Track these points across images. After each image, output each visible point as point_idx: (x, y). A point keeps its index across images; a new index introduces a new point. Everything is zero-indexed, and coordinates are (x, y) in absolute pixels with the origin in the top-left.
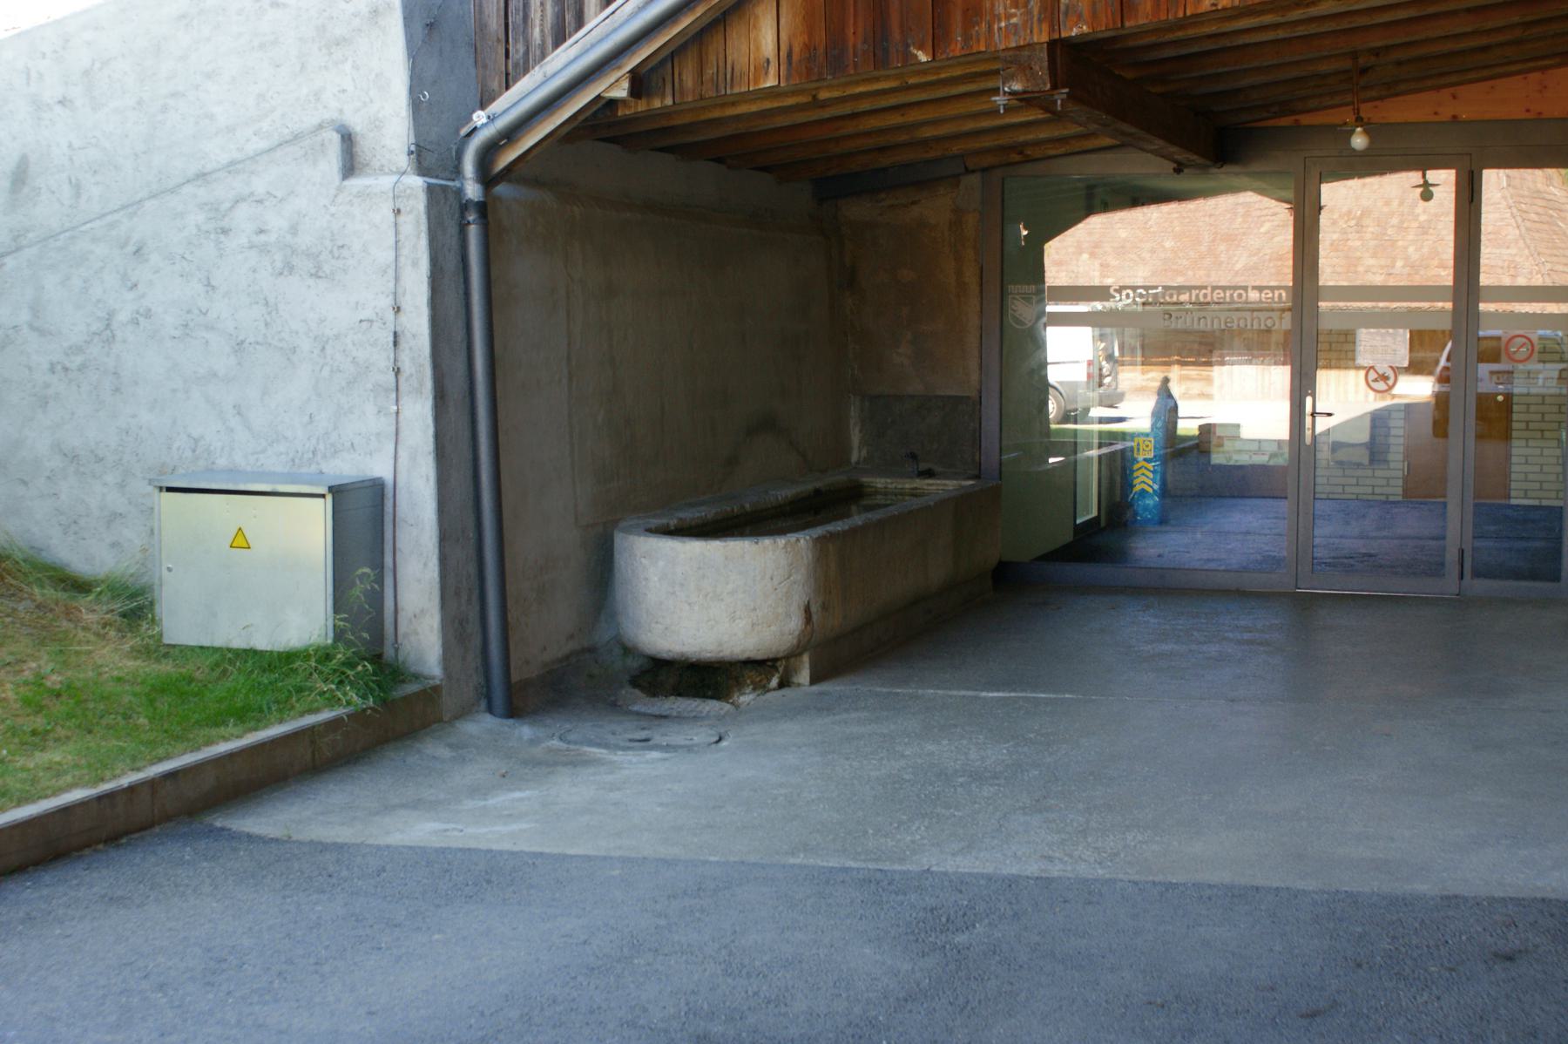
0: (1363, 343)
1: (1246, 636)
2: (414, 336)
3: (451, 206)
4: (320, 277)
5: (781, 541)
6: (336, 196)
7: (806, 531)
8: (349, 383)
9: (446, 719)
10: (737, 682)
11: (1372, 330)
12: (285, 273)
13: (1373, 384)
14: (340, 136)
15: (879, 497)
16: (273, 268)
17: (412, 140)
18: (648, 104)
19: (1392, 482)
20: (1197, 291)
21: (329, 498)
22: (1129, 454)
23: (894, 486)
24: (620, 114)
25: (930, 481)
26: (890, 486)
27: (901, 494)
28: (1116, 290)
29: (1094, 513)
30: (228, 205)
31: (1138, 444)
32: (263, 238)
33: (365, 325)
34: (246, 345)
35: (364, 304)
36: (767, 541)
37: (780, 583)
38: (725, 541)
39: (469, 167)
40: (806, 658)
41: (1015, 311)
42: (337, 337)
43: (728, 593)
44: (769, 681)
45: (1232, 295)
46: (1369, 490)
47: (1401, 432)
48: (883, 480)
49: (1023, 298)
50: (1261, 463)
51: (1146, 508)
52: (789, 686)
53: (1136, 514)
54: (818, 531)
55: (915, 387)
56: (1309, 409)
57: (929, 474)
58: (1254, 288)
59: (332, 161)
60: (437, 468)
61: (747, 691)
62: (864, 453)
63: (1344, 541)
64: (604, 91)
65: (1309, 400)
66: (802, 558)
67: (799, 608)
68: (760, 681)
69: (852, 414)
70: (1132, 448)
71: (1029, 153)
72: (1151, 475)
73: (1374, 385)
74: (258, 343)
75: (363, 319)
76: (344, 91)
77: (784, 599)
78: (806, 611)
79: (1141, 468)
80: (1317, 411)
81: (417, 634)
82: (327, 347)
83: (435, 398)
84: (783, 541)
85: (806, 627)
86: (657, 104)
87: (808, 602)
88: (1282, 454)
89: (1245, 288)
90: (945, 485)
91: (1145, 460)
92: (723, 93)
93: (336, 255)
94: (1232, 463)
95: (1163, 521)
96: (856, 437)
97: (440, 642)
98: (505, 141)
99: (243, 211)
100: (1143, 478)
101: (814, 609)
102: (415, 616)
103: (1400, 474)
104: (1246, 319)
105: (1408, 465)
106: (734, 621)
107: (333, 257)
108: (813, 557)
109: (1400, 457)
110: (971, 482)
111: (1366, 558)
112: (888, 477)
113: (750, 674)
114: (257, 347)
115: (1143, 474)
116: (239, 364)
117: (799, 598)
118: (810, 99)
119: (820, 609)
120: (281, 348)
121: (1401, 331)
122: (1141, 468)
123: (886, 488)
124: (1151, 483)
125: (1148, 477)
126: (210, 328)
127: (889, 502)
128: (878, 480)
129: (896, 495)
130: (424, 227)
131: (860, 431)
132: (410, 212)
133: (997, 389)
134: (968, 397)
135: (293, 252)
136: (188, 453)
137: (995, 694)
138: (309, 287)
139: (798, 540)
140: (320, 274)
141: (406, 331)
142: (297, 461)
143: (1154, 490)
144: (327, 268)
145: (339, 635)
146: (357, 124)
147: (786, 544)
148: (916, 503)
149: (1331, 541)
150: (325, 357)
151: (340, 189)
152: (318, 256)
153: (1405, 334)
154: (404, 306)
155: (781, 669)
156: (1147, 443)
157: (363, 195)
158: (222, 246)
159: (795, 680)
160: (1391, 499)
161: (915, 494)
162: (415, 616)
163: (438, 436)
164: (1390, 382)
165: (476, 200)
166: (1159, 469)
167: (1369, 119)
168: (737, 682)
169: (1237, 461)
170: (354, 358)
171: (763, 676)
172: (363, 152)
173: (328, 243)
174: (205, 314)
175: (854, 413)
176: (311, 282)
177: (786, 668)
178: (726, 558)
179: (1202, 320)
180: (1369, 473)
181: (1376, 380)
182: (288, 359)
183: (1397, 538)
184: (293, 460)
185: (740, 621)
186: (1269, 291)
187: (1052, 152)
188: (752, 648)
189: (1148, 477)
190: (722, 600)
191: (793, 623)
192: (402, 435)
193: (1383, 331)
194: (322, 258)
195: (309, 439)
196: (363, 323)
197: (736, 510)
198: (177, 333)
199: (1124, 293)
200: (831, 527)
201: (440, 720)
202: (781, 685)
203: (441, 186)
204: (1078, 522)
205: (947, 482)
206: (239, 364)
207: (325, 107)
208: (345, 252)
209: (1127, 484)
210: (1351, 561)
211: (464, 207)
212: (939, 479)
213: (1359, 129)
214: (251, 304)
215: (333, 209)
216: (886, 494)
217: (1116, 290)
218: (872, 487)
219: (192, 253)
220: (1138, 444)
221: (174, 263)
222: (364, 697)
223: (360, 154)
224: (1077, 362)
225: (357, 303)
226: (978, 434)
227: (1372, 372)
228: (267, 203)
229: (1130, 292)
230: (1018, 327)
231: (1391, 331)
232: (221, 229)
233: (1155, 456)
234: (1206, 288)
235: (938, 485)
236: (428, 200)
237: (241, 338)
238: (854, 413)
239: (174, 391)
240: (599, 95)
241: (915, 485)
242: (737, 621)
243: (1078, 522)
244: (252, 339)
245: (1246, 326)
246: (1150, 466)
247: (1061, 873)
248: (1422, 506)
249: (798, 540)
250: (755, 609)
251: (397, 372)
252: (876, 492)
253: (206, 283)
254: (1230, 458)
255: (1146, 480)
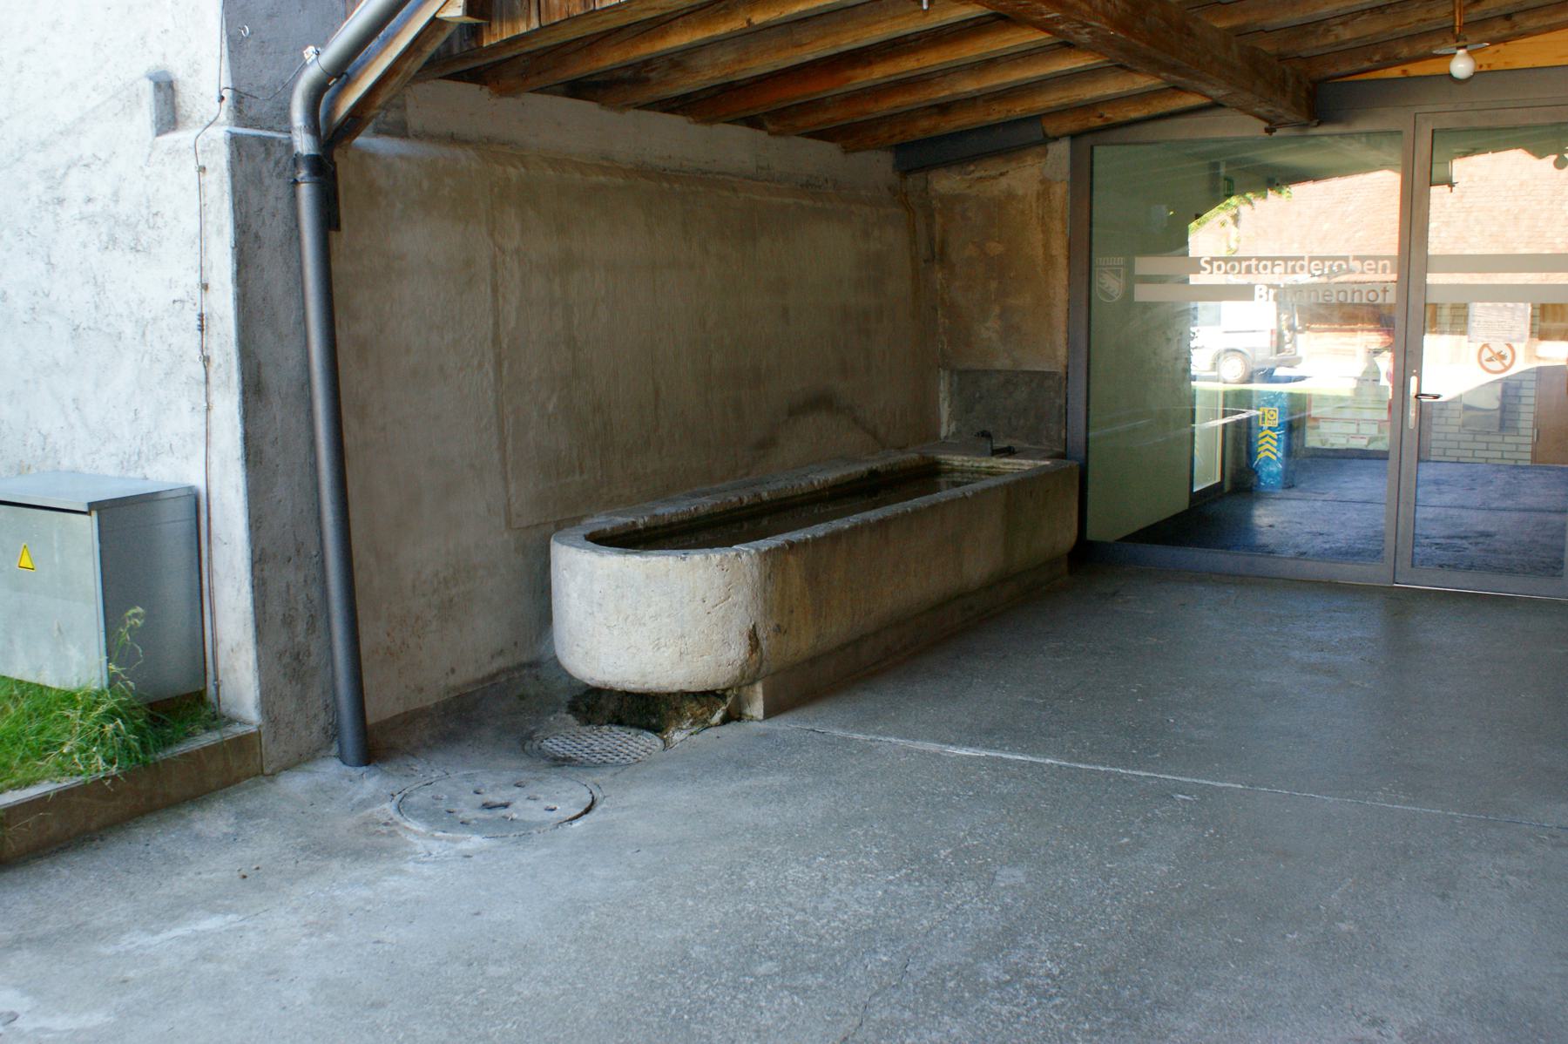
0: (1477, 319)
1: (1315, 657)
2: (221, 319)
3: (277, 163)
4: (138, 251)
5: (716, 556)
6: (150, 155)
7: (751, 544)
8: (166, 374)
9: (267, 771)
10: (678, 713)
11: (1488, 304)
12: (110, 247)
13: (1486, 364)
14: (152, 83)
15: (956, 474)
16: (100, 242)
17: (226, 81)
18: (513, 29)
19: (1522, 448)
20: (1293, 263)
21: (94, 514)
22: (1253, 423)
23: (970, 463)
24: (485, 45)
25: (1006, 460)
26: (966, 464)
27: (977, 472)
28: (1206, 262)
29: (1218, 479)
30: (62, 171)
31: (1264, 414)
32: (91, 208)
33: (178, 305)
34: (80, 330)
35: (176, 282)
36: (697, 557)
37: (713, 607)
38: (646, 557)
39: (298, 115)
40: (759, 688)
41: (1102, 284)
42: (155, 320)
43: (651, 617)
44: (712, 714)
45: (1331, 267)
46: (1499, 455)
47: (1533, 393)
48: (960, 458)
49: (1111, 271)
50: (1360, 447)
51: (1269, 475)
52: (739, 719)
53: (1259, 480)
54: (766, 544)
55: (1002, 363)
56: (1413, 390)
57: (1009, 452)
58: (1356, 258)
59: (145, 115)
60: (247, 476)
61: (684, 727)
62: (953, 428)
63: (1464, 513)
64: (438, 11)
65: (1413, 381)
66: (745, 576)
67: (741, 634)
68: (702, 714)
69: (942, 388)
70: (1257, 417)
71: (1109, 115)
72: (1275, 443)
73: (1491, 366)
74: (90, 328)
75: (176, 299)
76: (166, 31)
77: (720, 624)
78: (750, 638)
79: (1265, 436)
80: (1423, 392)
81: (235, 670)
82: (147, 332)
83: (244, 393)
84: (718, 557)
85: (751, 655)
86: (522, 29)
87: (754, 626)
88: (1382, 438)
89: (1346, 259)
90: (1022, 465)
91: (1270, 428)
92: (592, 8)
93: (151, 225)
94: (1328, 446)
95: (1289, 485)
96: (945, 411)
97: (257, 682)
98: (335, 80)
99: (75, 177)
100: (1267, 446)
101: (761, 634)
102: (232, 650)
103: (1529, 440)
104: (1346, 292)
105: (1538, 432)
106: (659, 649)
107: (149, 227)
108: (760, 574)
109: (1530, 424)
110: (1047, 463)
111: (1481, 540)
112: (966, 455)
113: (691, 708)
114: (90, 332)
115: (1268, 442)
116: (76, 352)
117: (740, 622)
118: (745, 25)
119: (771, 634)
120: (109, 334)
121: (1522, 305)
122: (1265, 436)
123: (962, 465)
124: (1275, 451)
125: (1272, 445)
126: (52, 312)
127: (965, 480)
128: (955, 458)
129: (972, 473)
130: (227, 187)
131: (949, 406)
132: (214, 170)
133: (1084, 365)
134: (1055, 374)
135: (116, 222)
136: (39, 452)
137: (964, 752)
138: (130, 262)
139: (738, 555)
140: (140, 248)
141: (214, 315)
142: (125, 464)
143: (1278, 458)
144: (144, 240)
145: (113, 679)
146: (179, 71)
147: (721, 560)
148: (992, 482)
149: (1452, 512)
150: (146, 345)
151: (153, 147)
152: (136, 227)
153: (1526, 309)
154: (211, 284)
155: (729, 700)
156: (1272, 412)
157: (173, 152)
158: (58, 219)
159: (748, 711)
160: (1520, 463)
161: (991, 473)
162: (232, 650)
163: (247, 438)
164: (1507, 362)
165: (305, 153)
166: (1282, 437)
167: (1489, 65)
168: (678, 713)
169: (1333, 444)
170: (170, 345)
171: (705, 708)
172: (184, 102)
173: (144, 211)
174: (48, 296)
175: (943, 387)
176: (131, 256)
177: (737, 699)
178: (648, 577)
179: (1356, 294)
180: (1499, 439)
181: (1490, 360)
182: (116, 347)
183: (1520, 510)
184: (122, 462)
185: (665, 649)
186: (1371, 262)
187: (1134, 115)
188: (681, 681)
189: (1272, 445)
190: (644, 624)
191: (732, 651)
192: (214, 438)
193: (1500, 305)
194: (140, 228)
195: (134, 438)
196: (177, 304)
197: (746, 500)
198: (26, 318)
199: (1215, 264)
200: (797, 536)
201: (260, 773)
202: (726, 720)
203: (259, 137)
204: (1195, 490)
205: (1023, 461)
206: (76, 352)
207: (150, 52)
208: (160, 221)
209: (1251, 453)
210: (1465, 543)
211: (296, 160)
212: (1017, 458)
213: (1461, 52)
214: (83, 284)
215: (148, 171)
216: (962, 472)
217: (1206, 262)
218: (948, 464)
219: (35, 227)
220: (1264, 414)
221: (22, 240)
222: (111, 762)
223: (182, 104)
224: (1254, 331)
225: (170, 280)
226: (1064, 411)
227: (1486, 350)
228: (93, 167)
229: (1237, 264)
230: (1104, 300)
231: (1510, 305)
232: (58, 199)
233: (1279, 425)
234: (1302, 258)
235: (1014, 464)
236: (232, 154)
237: (77, 322)
238: (943, 387)
239: (26, 381)
240: (434, 19)
241: (991, 464)
242: (662, 649)
243: (1195, 490)
244: (84, 325)
245: (1346, 299)
246: (1274, 435)
247: (1442, 510)
248: (1550, 472)
249: (738, 555)
250: (682, 636)
251: (206, 360)
252: (953, 471)
253: (47, 261)
254: (1327, 441)
255: (1270, 450)
